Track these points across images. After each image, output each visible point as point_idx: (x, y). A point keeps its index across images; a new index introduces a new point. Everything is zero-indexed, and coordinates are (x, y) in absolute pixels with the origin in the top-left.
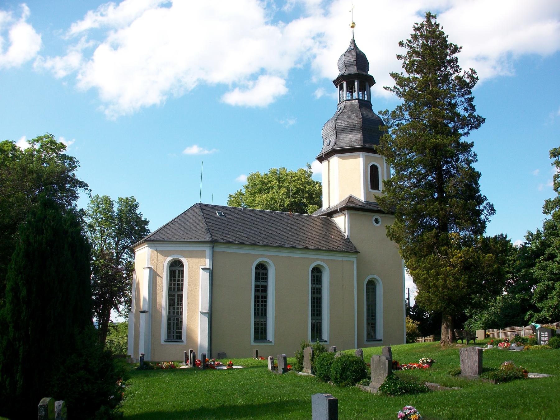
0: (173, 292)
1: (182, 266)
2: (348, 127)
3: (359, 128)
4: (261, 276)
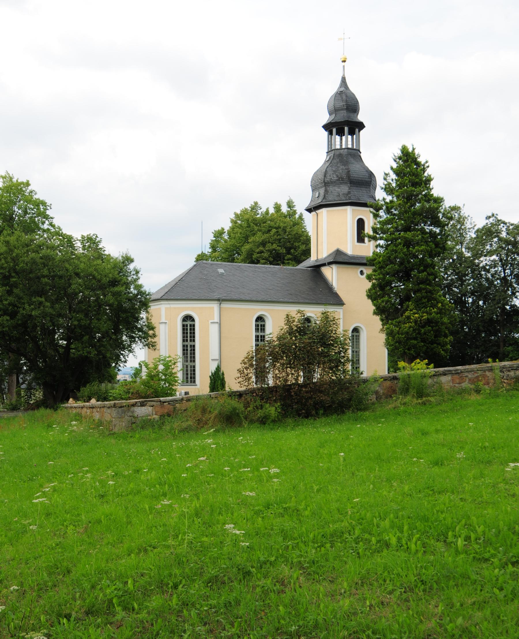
1: (193, 320)
4: (260, 327)
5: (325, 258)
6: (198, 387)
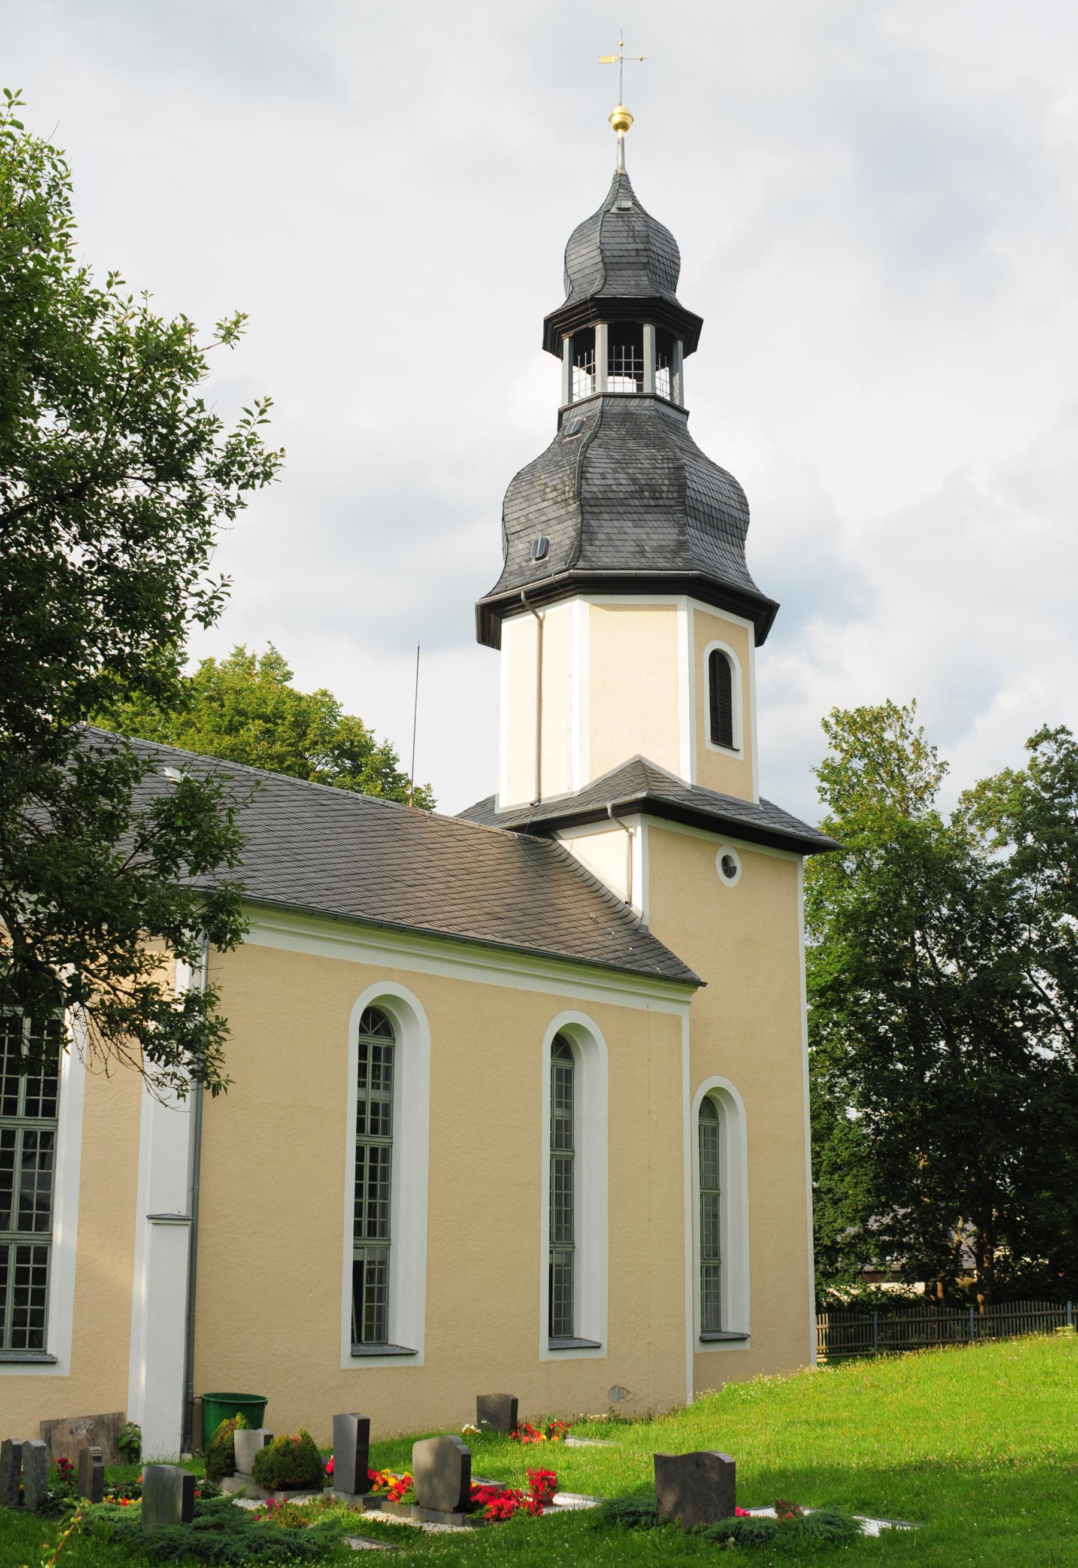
0: (819, 1287)
2: (632, 495)
3: (672, 502)
5: (584, 794)
6: (64, 1368)
